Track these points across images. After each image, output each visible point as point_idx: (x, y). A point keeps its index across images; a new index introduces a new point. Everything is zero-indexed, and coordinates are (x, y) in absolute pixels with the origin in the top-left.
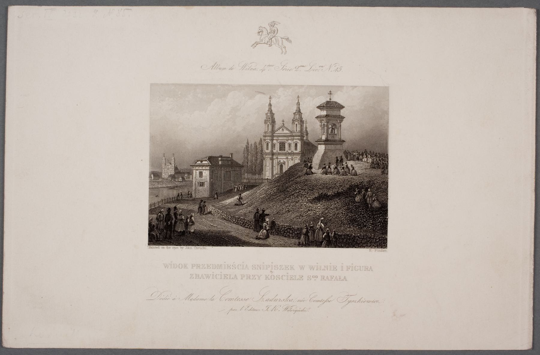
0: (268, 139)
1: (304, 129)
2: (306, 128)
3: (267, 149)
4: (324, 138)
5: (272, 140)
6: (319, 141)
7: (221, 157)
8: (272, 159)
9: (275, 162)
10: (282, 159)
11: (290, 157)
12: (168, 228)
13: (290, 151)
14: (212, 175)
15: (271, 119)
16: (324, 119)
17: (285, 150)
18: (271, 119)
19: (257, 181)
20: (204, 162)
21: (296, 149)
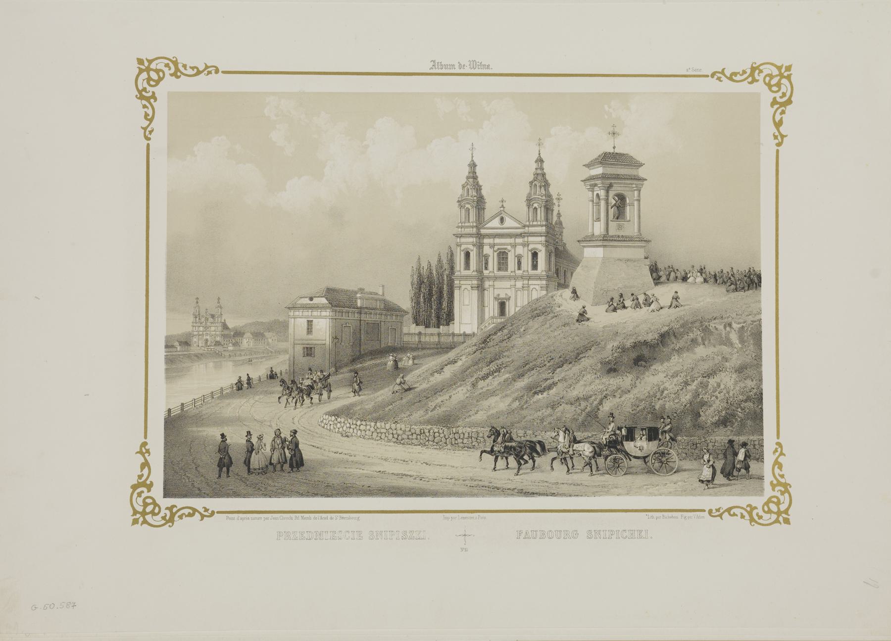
0: (469, 243)
1: (555, 219)
2: (559, 215)
3: (467, 266)
4: (599, 229)
5: (480, 246)
6: (589, 240)
7: (361, 290)
8: (481, 288)
9: (489, 297)
10: (503, 288)
11: (519, 284)
12: (208, 466)
13: (519, 273)
14: (503, 490)
15: (475, 200)
16: (599, 182)
17: (507, 270)
18: (475, 200)
19: (443, 339)
20: (316, 301)
21: (535, 267)
